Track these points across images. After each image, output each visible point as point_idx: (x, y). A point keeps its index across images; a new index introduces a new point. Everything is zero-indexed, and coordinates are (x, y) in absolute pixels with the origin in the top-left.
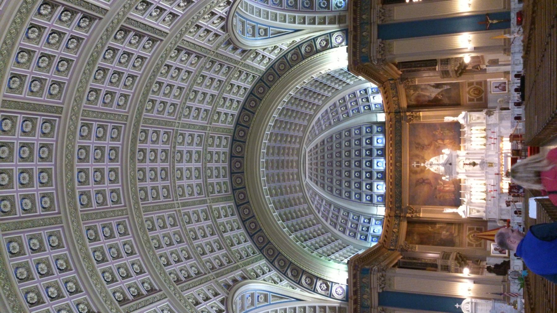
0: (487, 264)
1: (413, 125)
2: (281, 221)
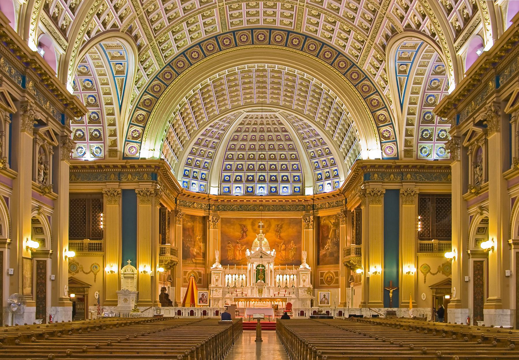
1: (301, 222)
2: (201, 87)
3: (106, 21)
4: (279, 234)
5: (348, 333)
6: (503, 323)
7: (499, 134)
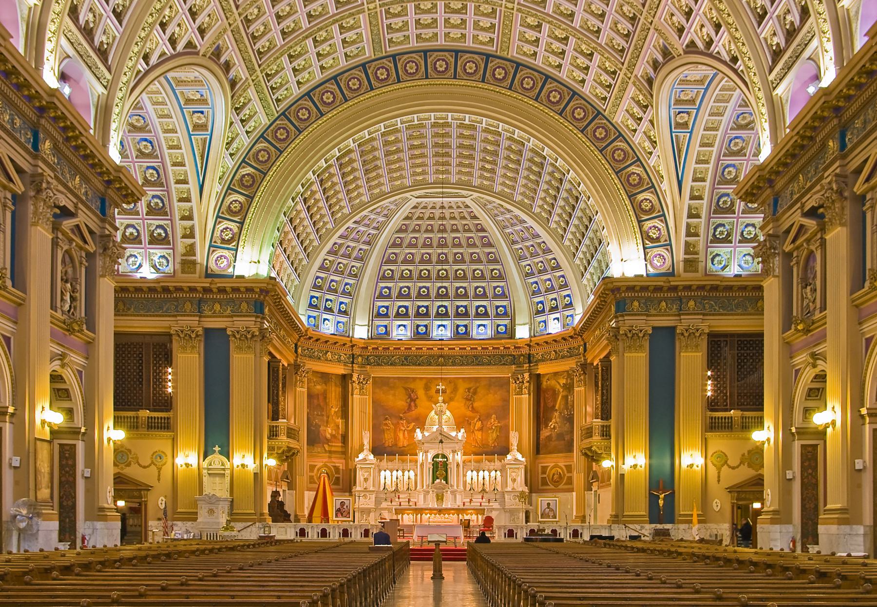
2: (338, 154)
3: (176, 36)
4: (472, 404)
5: (589, 565)
6: (852, 548)
7: (845, 229)
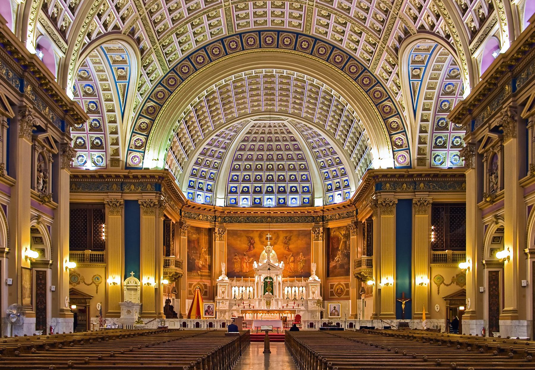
0: (173, 299)
2: (206, 94)
3: (107, 22)
4: (288, 246)
5: (359, 344)
6: (519, 334)
7: (515, 139)
